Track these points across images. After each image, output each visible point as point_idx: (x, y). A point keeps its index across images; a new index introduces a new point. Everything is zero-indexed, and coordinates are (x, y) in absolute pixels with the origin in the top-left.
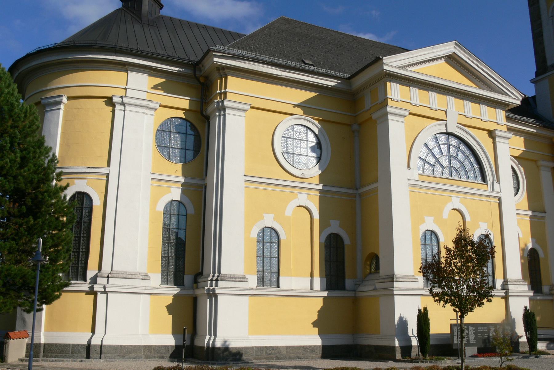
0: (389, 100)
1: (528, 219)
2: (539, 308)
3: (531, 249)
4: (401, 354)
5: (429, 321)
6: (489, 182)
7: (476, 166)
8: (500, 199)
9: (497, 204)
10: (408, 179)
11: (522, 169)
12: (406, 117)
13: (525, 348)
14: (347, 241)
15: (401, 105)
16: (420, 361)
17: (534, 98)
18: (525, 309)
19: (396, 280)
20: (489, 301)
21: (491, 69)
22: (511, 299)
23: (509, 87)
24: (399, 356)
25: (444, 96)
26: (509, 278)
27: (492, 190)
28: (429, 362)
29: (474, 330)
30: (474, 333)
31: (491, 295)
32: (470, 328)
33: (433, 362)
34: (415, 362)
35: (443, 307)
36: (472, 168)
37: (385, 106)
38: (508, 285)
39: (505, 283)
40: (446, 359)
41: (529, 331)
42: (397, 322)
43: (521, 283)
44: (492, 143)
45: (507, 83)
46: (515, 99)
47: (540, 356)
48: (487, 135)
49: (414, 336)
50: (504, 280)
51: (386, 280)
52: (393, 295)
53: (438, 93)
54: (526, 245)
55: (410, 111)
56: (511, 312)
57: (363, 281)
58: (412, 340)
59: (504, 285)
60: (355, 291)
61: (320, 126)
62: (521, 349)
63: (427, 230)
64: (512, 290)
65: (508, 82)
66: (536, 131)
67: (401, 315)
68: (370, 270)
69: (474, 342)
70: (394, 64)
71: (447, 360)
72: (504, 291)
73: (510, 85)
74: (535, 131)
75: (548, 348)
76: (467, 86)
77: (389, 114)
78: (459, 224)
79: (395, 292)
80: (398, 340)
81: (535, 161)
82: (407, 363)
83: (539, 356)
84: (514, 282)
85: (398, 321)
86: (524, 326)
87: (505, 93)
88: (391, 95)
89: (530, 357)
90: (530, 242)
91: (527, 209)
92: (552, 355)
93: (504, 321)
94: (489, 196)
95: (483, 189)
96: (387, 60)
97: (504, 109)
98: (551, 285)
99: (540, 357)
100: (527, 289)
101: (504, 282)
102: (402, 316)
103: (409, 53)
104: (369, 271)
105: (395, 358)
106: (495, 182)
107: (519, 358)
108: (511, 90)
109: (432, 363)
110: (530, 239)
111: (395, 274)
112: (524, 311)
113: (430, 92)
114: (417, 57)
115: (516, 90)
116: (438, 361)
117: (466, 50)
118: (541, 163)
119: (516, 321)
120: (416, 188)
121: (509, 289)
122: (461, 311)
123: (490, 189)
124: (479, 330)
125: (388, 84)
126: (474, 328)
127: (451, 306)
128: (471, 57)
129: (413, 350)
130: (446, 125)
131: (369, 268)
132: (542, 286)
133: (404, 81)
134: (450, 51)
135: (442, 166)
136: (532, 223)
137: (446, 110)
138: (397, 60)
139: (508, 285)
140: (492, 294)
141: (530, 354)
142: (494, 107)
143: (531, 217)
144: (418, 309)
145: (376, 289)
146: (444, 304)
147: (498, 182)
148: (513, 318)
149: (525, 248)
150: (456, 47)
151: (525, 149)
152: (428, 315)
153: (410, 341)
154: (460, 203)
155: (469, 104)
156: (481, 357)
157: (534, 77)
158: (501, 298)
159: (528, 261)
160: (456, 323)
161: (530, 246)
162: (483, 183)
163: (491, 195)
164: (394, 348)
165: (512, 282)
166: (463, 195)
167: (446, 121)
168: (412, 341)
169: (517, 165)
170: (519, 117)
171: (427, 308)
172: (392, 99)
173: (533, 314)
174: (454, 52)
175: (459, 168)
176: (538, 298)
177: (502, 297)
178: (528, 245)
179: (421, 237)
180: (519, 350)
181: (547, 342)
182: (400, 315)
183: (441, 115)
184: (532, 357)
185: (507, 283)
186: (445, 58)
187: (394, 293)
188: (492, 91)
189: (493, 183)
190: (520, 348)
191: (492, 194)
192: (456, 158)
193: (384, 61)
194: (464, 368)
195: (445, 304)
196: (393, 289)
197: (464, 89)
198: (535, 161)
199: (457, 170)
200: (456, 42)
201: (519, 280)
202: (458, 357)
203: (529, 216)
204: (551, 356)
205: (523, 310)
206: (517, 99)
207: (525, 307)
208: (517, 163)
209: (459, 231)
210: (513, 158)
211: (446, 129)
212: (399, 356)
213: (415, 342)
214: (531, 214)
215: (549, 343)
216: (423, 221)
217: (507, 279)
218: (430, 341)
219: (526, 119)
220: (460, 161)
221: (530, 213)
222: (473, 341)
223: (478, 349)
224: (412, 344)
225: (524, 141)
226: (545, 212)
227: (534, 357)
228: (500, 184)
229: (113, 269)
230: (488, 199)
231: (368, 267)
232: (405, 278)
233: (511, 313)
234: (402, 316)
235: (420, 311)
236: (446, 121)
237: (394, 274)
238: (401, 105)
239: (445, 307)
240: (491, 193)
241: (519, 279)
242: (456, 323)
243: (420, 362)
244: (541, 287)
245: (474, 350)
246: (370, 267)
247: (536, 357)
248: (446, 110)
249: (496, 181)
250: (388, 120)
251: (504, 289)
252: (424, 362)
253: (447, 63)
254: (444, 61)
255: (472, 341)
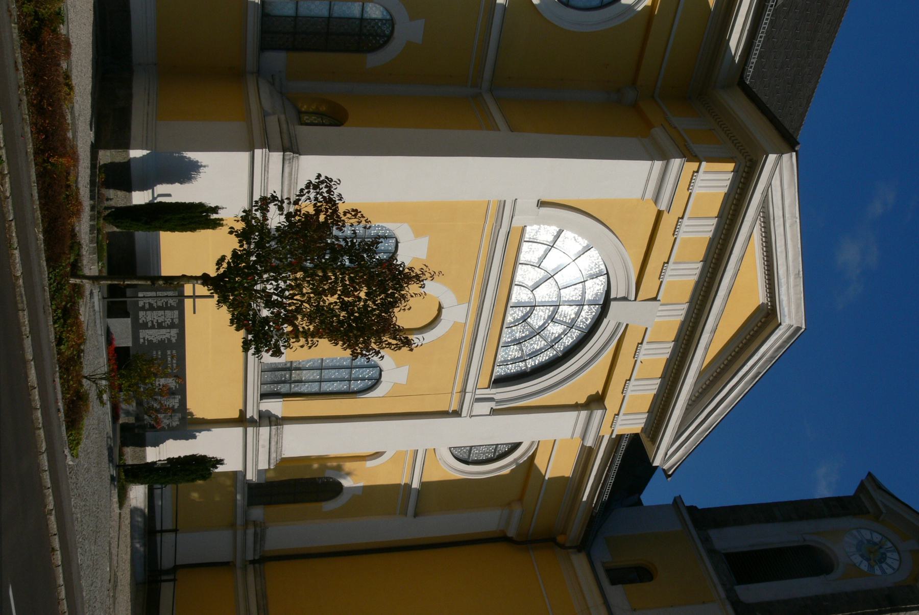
0: (695, 165)
1: (404, 480)
2: (217, 499)
3: (340, 485)
4: (111, 163)
5: (191, 231)
6: (494, 391)
7: (531, 363)
8: (457, 414)
9: (446, 409)
10: (516, 199)
11: (507, 471)
12: (654, 205)
13: (130, 456)
14: (375, 60)
15: (682, 193)
16: (95, 203)
17: (639, 503)
18: (217, 460)
19: (287, 158)
20: (246, 346)
21: (736, 404)
22: (239, 431)
23: (694, 439)
24: (106, 156)
25: (687, 297)
26: (284, 428)
27: (476, 397)
28: (92, 223)
29: (169, 340)
30: (162, 342)
31: (261, 351)
32: (174, 332)
33: (93, 233)
34: (91, 191)
35: (232, 228)
36: (527, 355)
37: (683, 154)
38: (270, 426)
39: (273, 419)
40: (102, 267)
41: (169, 465)
42: (188, 156)
43: (273, 455)
44: (577, 402)
45: (702, 438)
46: (666, 454)
47: (115, 486)
48: (594, 393)
49: (154, 198)
50: (280, 418)
51: (285, 136)
52: (250, 148)
53: (697, 283)
54: (349, 474)
55: (665, 213)
56: (210, 430)
57: (281, 93)
58: (145, 191)
59: (269, 418)
60: (259, 73)
61: (639, 9)
62: (129, 451)
63: (397, 243)
64: (258, 434)
65: (703, 440)
66: (584, 501)
67: (205, 166)
68: (306, 113)
69: (142, 341)
70: (776, 182)
71: (98, 266)
72: (256, 417)
73: (696, 445)
74: (585, 499)
75: (134, 511)
76: (707, 349)
77: (665, 162)
78: (437, 273)
79: (258, 153)
80: (144, 156)
81: (520, 500)
82: (88, 171)
83: (116, 483)
84: (276, 440)
85: (190, 158)
86: (180, 457)
87: (681, 431)
88: (705, 172)
89: (111, 465)
90: (354, 484)
91: (425, 479)
92: (118, 515)
93: (191, 414)
94: (465, 389)
95: (478, 380)
96: (789, 162)
97: (645, 432)
98: (264, 523)
99: (113, 488)
100: (259, 469)
101: (277, 417)
102: (201, 171)
103: (797, 218)
104: (303, 110)
105: (101, 149)
106: (492, 405)
107: (109, 440)
108: (686, 447)
109: (90, 231)
110: (361, 484)
111: (302, 156)
112: (213, 458)
113: (700, 265)
114: (783, 237)
115: (684, 458)
116: (95, 245)
117: (783, 351)
118: (517, 510)
119: (190, 440)
120: (493, 220)
121: (261, 428)
122: (220, 277)
123: (481, 393)
124: (169, 352)
125: (731, 166)
126: (174, 340)
127: (234, 253)
128: (766, 362)
129: (120, 193)
130: (625, 299)
131: (311, 110)
132: (262, 506)
133: (735, 198)
134: (785, 316)
135: (537, 286)
136: (397, 487)
137: (659, 300)
138: (786, 186)
139: (270, 426)
140: (264, 354)
141: (118, 467)
142: (651, 411)
143: (408, 487)
144: (219, 205)
145: (264, 115)
146: (236, 232)
147: (494, 412)
148: (197, 434)
149: (343, 473)
150: (792, 329)
151: (548, 478)
152: (204, 228)
153: (143, 188)
154: (455, 322)
155: (666, 353)
156: (108, 354)
157: (687, 504)
158: (241, 411)
159: (315, 478)
160: (186, 294)
161: (347, 483)
162: (493, 379)
163: (467, 394)
164: (127, 146)
165: (275, 435)
166: (471, 330)
167: (635, 300)
168: (142, 192)
169: (515, 460)
170: (615, 468)
171: (220, 228)
172: (697, 172)
173: (208, 478)
174: (780, 324)
175: (529, 324)
176: (239, 497)
177: (243, 413)
178: (349, 478)
179: (382, 227)
180: (128, 446)
181: (146, 510)
182: (203, 164)
183: (648, 288)
184: (111, 468)
185: (273, 423)
186: (769, 304)
187: (256, 150)
188: (690, 402)
189: (491, 399)
190: (131, 447)
191: (468, 397)
192: (552, 318)
193: (786, 157)
194: (78, 281)
195: (237, 236)
196: (266, 148)
197: (701, 341)
198: (520, 500)
199: (524, 319)
200: (803, 330)
201: (279, 450)
202: (106, 296)
203: (409, 482)
204: (117, 511)
205: (215, 457)
206: (666, 459)
207: (222, 460)
208: (521, 461)
209: (419, 272)
210: (530, 454)
211: (616, 299)
212: (106, 156)
213: (140, 198)
214: (413, 487)
215: (144, 513)
216: (418, 233)
217: (282, 425)
218: (142, 230)
219: (611, 481)
220: (543, 327)
221: (415, 485)
222: (144, 338)
223: (127, 349)
224: (135, 191)
225: (563, 477)
226: (416, 515)
227: (112, 473)
228: (489, 416)
229: (288, 429)
230: (458, 387)
231: (313, 108)
232: (290, 180)
233: (209, 430)
234: (202, 170)
235: (215, 210)
236: (633, 298)
237: (300, 155)
238: (682, 193)
239: (231, 233)
240: (471, 394)
241: (281, 451)
242: (186, 294)
243: (92, 202)
244: (261, 504)
245: (124, 339)
246: (314, 113)
247: (112, 477)
248: (659, 300)
249: (495, 408)
250: (652, 158)
251: (260, 417)
252: (92, 213)
253: (757, 308)
254: (763, 303)
255: (145, 334)
